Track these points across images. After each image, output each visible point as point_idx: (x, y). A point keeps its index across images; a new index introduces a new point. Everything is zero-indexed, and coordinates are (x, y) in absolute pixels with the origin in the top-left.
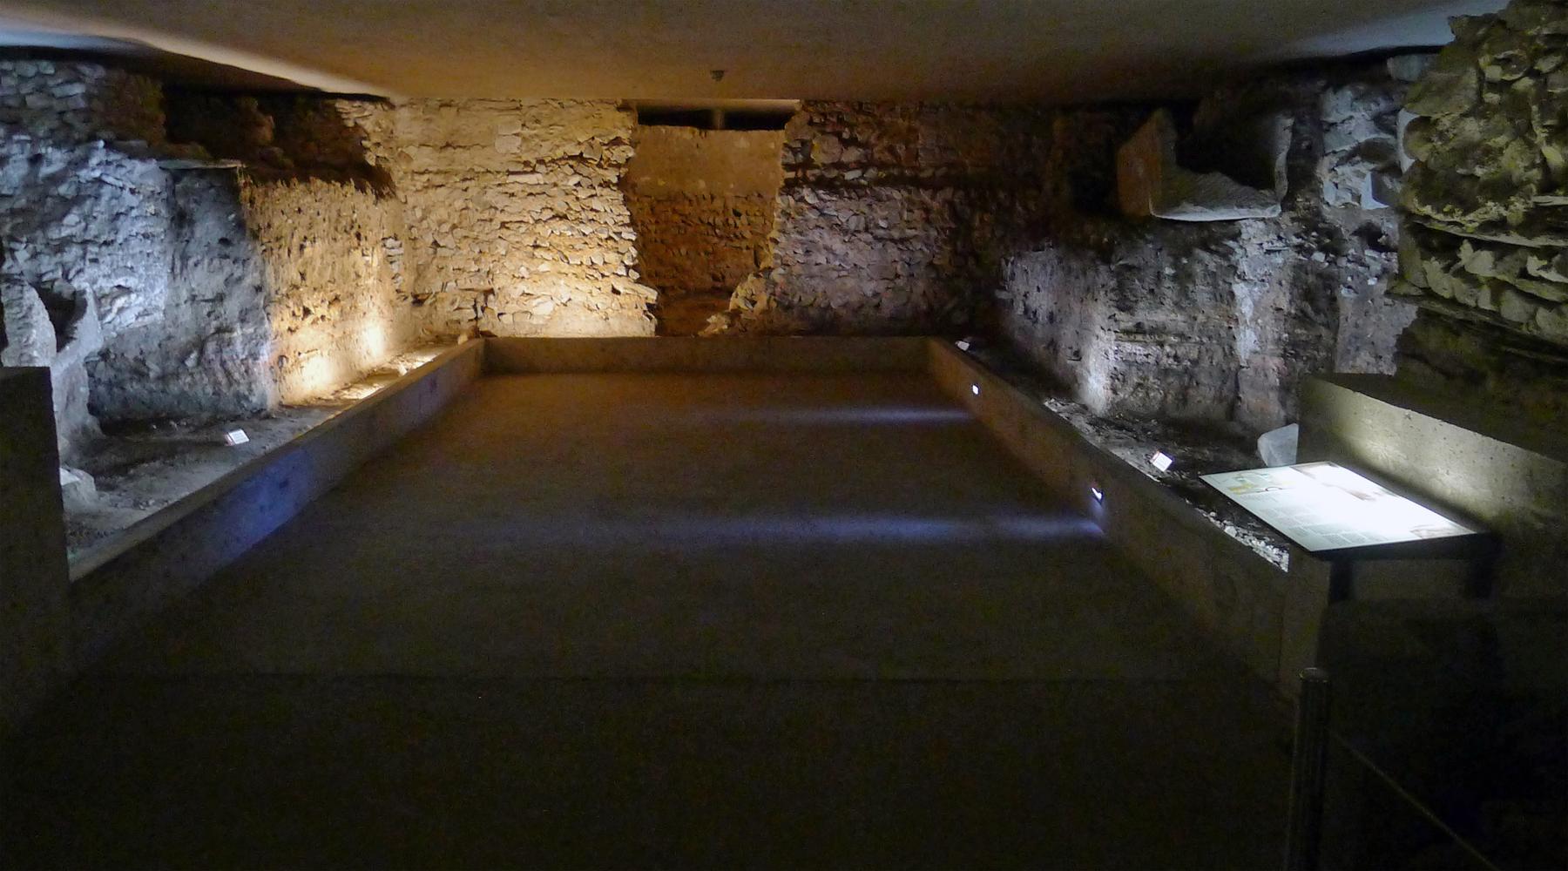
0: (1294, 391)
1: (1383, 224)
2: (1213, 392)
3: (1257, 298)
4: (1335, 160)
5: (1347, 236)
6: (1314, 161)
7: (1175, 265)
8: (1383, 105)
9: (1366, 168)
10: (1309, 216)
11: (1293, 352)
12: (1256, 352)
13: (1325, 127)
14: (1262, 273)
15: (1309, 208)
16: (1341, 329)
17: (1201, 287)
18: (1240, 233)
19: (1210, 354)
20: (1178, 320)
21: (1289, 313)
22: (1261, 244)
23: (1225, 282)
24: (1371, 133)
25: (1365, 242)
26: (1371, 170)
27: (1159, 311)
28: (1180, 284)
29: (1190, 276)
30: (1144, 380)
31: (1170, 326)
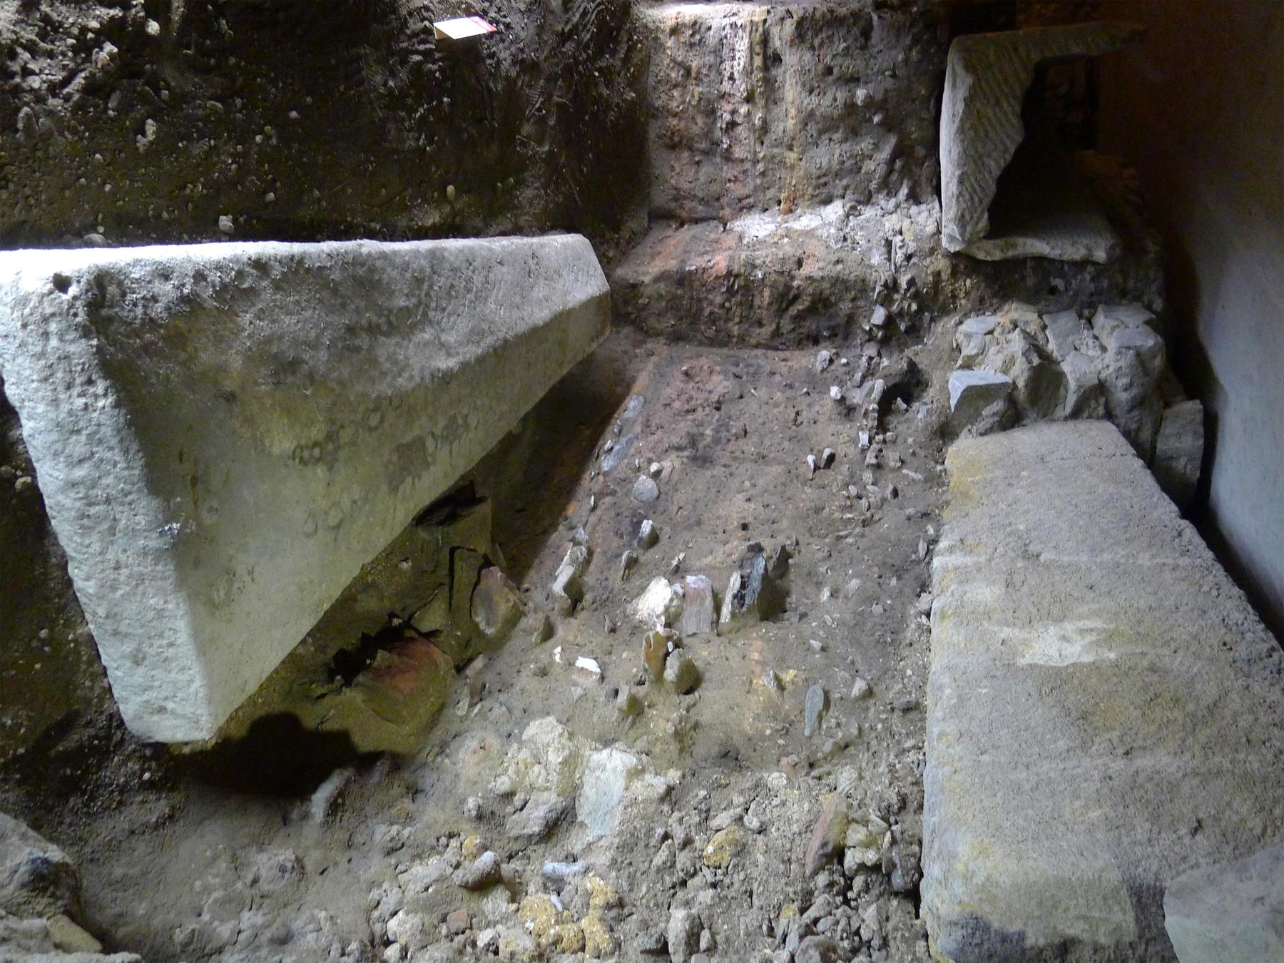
0: (679, 292)
1: (925, 404)
2: (686, 186)
3: (819, 232)
4: (1032, 328)
5: (909, 352)
6: (1031, 298)
7: (870, 103)
8: (1122, 397)
9: (1020, 374)
10: (941, 298)
11: (736, 287)
12: (741, 238)
13: (1086, 312)
14: (857, 238)
15: (954, 297)
16: (771, 353)
17: (838, 152)
18: (918, 203)
19: (741, 177)
20: (786, 122)
21: (793, 278)
22: (901, 233)
23: (846, 188)
24: (1078, 380)
25: (897, 379)
26: (1014, 383)
27: (799, 88)
28: (841, 118)
29: (854, 133)
30: (695, 79)
31: (777, 111)
